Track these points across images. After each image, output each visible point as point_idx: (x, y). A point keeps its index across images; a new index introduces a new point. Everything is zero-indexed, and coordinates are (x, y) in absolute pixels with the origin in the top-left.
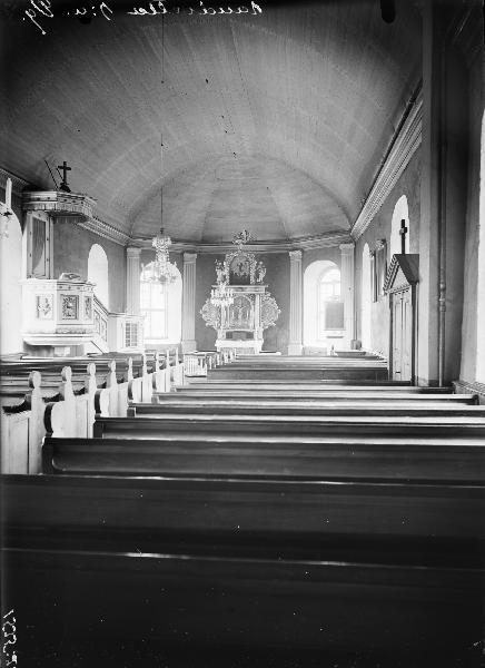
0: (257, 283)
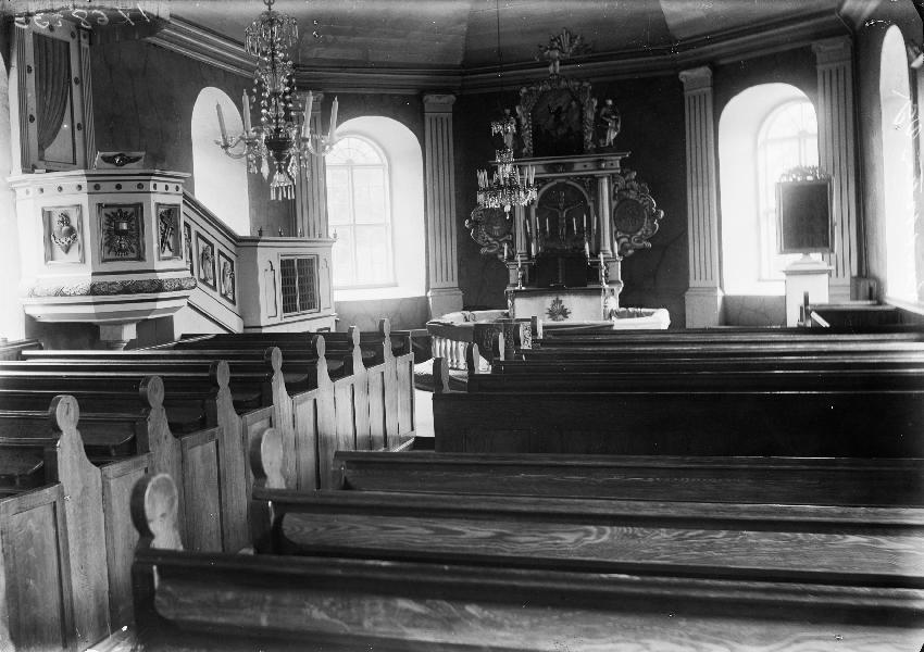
0: (599, 150)
